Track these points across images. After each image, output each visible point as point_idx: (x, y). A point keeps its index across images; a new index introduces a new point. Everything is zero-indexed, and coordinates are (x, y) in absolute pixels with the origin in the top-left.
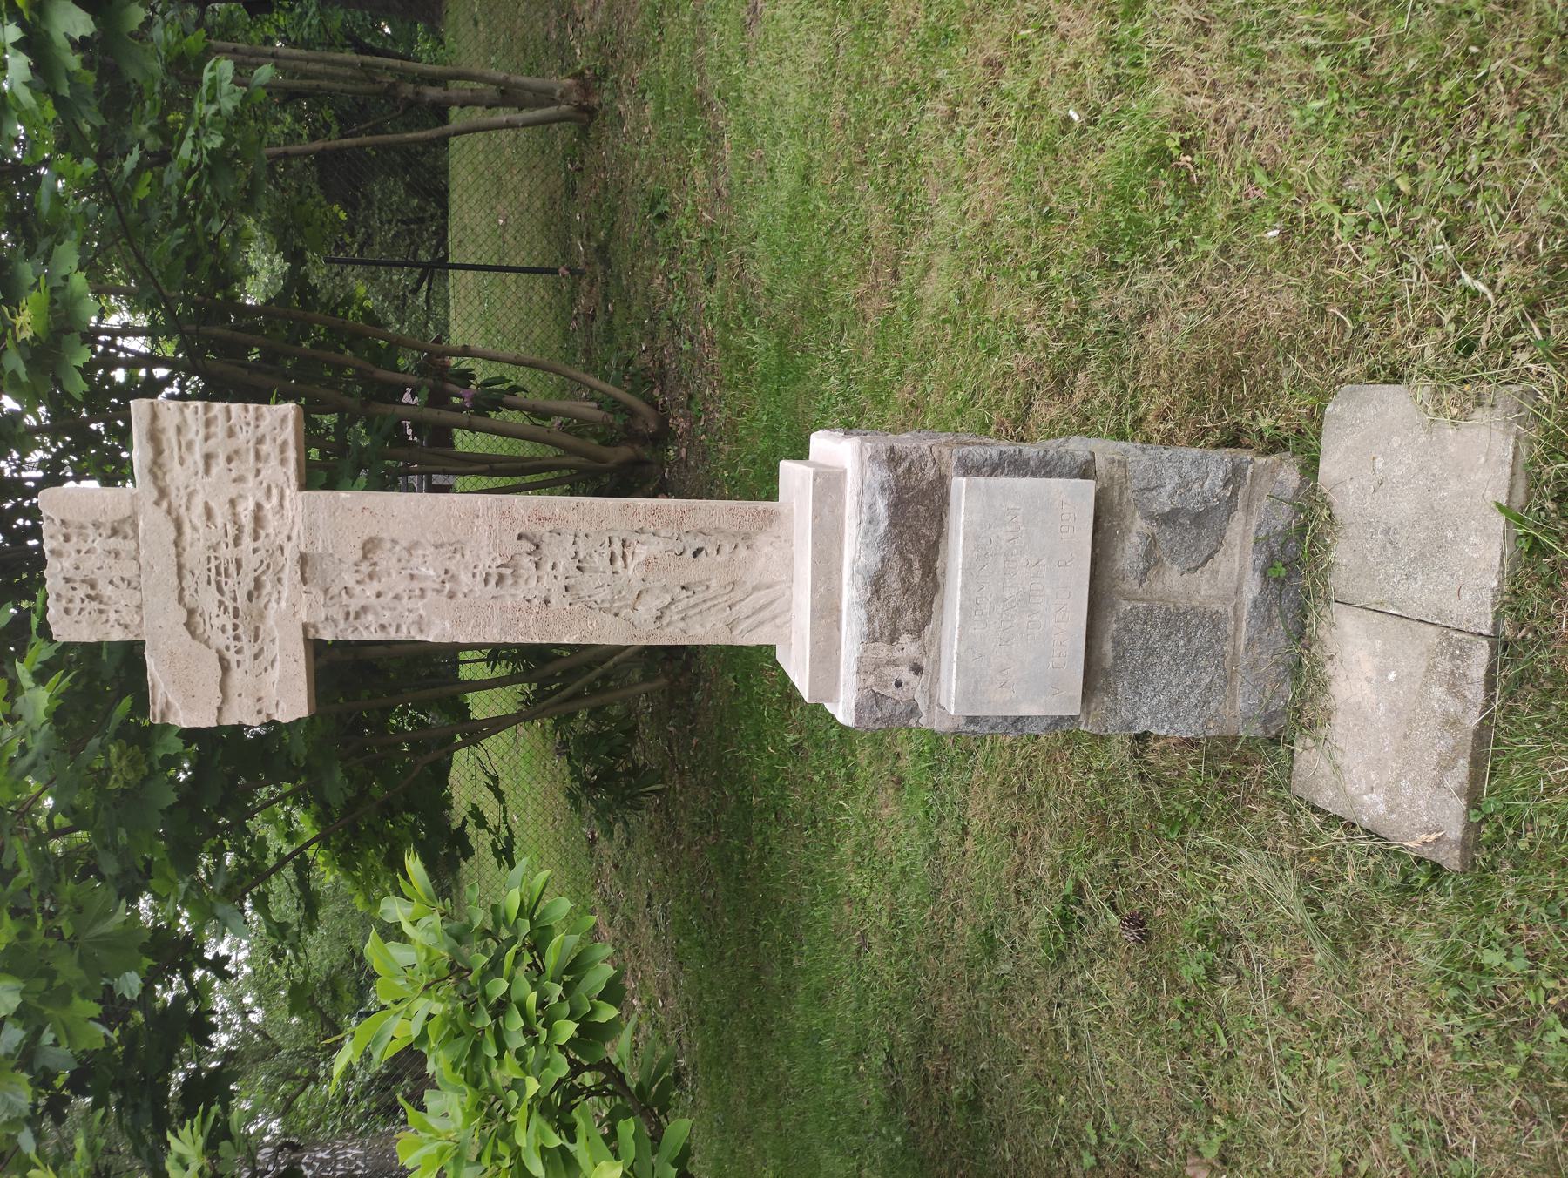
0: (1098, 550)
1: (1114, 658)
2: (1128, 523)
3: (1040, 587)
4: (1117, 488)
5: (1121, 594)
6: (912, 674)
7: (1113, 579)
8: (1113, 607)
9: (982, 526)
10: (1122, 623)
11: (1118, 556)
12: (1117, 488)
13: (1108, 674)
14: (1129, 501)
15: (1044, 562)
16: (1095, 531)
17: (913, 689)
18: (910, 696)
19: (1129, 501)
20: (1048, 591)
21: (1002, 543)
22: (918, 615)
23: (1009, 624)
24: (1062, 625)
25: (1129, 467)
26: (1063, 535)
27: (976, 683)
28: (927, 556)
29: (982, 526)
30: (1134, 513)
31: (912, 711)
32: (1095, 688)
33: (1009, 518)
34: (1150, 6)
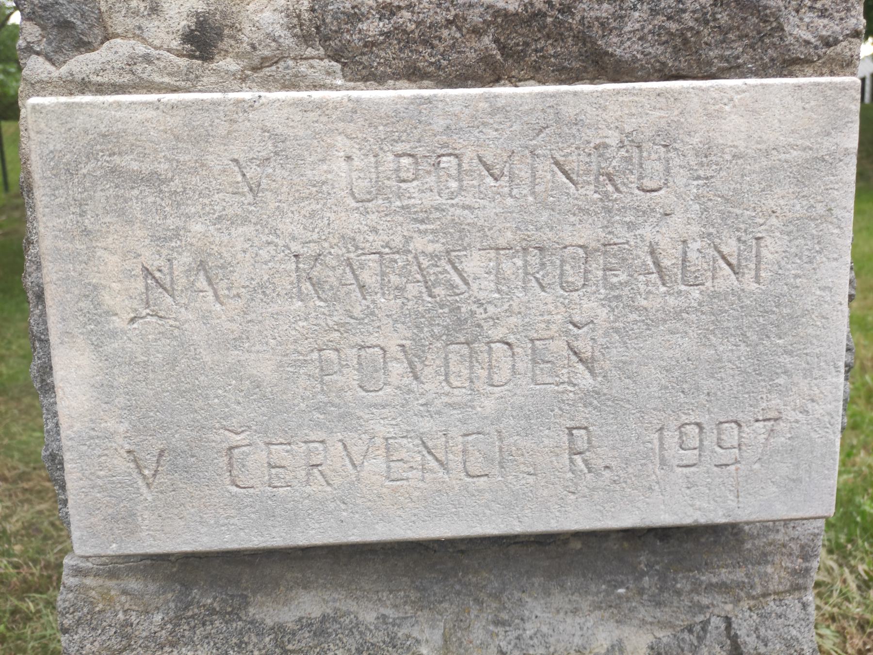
0: (577, 545)
1: (279, 629)
2: (642, 613)
3: (503, 374)
4: (739, 575)
5: (460, 623)
6: (183, 23)
7: (496, 596)
8: (420, 605)
9: (706, 152)
10: (379, 637)
11: (559, 599)
12: (739, 575)
13: (231, 615)
14: (702, 609)
15: (585, 380)
16: (664, 533)
17: (138, 34)
18: (119, 22)
19: (702, 609)
20: (489, 405)
21: (647, 231)
22: (373, 27)
23: (368, 277)
24: (376, 465)
25: (789, 599)
26: (672, 438)
27: (153, 180)
28: (557, 35)
29: (706, 152)
30: (670, 625)
31: (65, 25)
32: (187, 586)
33: (730, 247)
34: (2, 571)
